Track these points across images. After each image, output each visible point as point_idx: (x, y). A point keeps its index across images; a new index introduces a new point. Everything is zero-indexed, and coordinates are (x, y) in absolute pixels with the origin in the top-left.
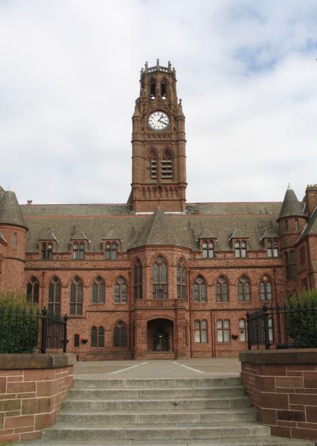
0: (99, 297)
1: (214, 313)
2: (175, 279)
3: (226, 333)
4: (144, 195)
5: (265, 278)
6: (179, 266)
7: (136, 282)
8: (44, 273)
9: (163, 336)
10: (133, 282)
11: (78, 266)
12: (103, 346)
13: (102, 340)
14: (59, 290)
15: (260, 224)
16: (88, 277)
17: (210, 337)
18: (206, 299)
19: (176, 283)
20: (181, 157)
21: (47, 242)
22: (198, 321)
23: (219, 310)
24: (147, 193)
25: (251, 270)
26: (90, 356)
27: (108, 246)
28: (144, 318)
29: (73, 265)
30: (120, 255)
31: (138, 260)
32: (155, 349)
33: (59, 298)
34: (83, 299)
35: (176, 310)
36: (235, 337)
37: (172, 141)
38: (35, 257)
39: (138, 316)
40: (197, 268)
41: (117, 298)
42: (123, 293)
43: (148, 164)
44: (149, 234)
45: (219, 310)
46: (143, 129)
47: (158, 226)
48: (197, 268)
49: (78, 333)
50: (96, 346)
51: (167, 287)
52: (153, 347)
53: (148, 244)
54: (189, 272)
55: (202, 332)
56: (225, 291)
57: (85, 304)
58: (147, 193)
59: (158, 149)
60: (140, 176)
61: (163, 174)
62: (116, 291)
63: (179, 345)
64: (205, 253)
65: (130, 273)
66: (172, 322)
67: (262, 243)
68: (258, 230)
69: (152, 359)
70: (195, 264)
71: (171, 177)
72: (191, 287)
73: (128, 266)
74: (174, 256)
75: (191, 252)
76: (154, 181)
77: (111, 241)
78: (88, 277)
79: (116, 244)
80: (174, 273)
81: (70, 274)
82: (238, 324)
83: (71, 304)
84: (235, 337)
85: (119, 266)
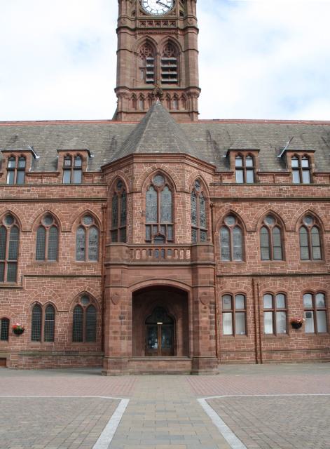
0: (47, 251)
1: (258, 281)
2: (188, 216)
3: (280, 317)
4: (135, 106)
6: (194, 195)
7: (115, 222)
9: (165, 319)
10: (110, 223)
11: (13, 196)
12: (52, 340)
17: (251, 325)
18: (243, 256)
19: (189, 223)
20: (190, 51)
22: (230, 295)
24: (139, 103)
26: (24, 360)
27: (68, 163)
28: (131, 281)
30: (88, 177)
31: (120, 183)
32: (149, 352)
34: (18, 254)
35: (193, 267)
36: (297, 325)
37: (178, 29)
39: (113, 279)
41: (81, 253)
42: (92, 243)
43: (141, 63)
44: (140, 138)
46: (134, 13)
49: (9, 317)
51: (173, 231)
52: (145, 347)
53: (137, 151)
54: (212, 207)
55: (236, 315)
57: (21, 264)
59: (157, 41)
61: (164, 76)
62: (79, 240)
63: (201, 342)
65: (104, 208)
66: (184, 294)
68: (324, 144)
70: (221, 192)
71: (175, 80)
73: (101, 195)
74: (186, 175)
75: (215, 173)
76: (151, 86)
77: (73, 154)
79: (82, 158)
80: (186, 206)
82: (302, 302)
84: (297, 325)
85: (85, 196)
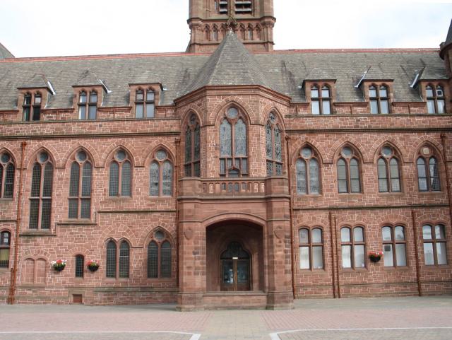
1: (335, 214)
2: (263, 149)
4: (208, 37)
5: (426, 151)
6: (269, 127)
7: (188, 156)
8: (24, 145)
10: (183, 157)
11: (85, 131)
12: (127, 276)
13: (126, 264)
14: (50, 175)
15: (405, 65)
16: (102, 151)
17: (328, 259)
18: (320, 188)
21: (33, 92)
22: (307, 229)
23: (344, 209)
24: (213, 34)
25: (401, 135)
27: (140, 97)
29: (75, 129)
30: (161, 111)
31: (193, 116)
32: (225, 287)
33: (49, 190)
35: (268, 200)
36: (375, 259)
38: (10, 118)
40: (302, 132)
41: (155, 188)
42: (165, 177)
44: (213, 70)
45: (344, 209)
47: (229, 58)
48: (302, 132)
49: (80, 252)
50: (115, 277)
52: (221, 282)
53: (210, 84)
54: (287, 139)
56: (354, 172)
57: (94, 200)
58: (213, 34)
60: (201, 8)
62: (152, 175)
64: (315, 105)
65: (177, 142)
67: (416, 90)
69: (216, 308)
70: (296, 124)
71: (249, 10)
72: (292, 166)
73: (174, 129)
74: (260, 107)
75: (291, 105)
76: (224, 16)
77: (145, 87)
78: (102, 151)
79: (154, 92)
80: (261, 140)
81: (71, 146)
82: (380, 235)
83: (70, 199)
84: (375, 259)
85: (158, 130)
